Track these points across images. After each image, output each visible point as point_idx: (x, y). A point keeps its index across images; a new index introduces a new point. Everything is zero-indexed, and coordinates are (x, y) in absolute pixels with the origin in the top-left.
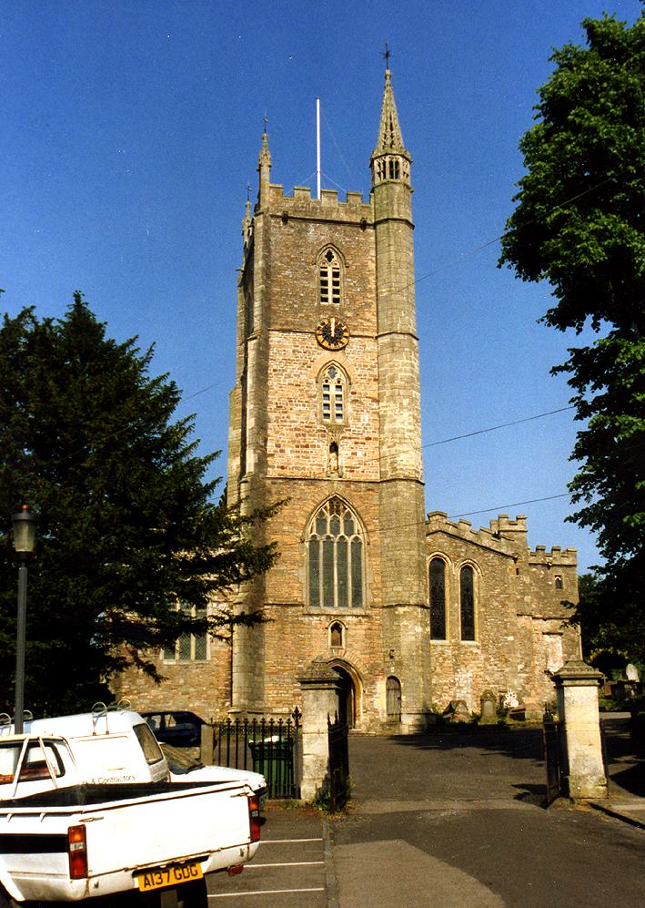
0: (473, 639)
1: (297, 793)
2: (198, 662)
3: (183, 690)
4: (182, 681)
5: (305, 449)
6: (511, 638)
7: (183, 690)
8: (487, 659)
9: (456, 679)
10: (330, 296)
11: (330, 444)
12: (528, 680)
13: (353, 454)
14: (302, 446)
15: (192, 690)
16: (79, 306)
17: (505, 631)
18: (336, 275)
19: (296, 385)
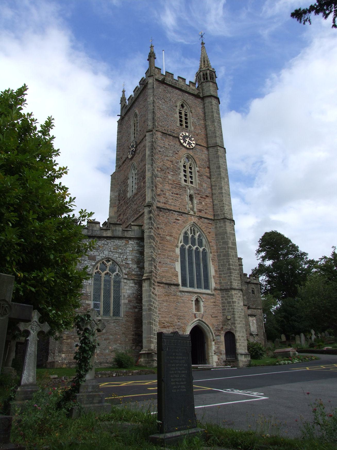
1: (235, 249)
2: (114, 318)
5: (176, 195)
13: (200, 203)
14: (175, 194)
15: (111, 337)
16: (22, 91)
19: (171, 161)
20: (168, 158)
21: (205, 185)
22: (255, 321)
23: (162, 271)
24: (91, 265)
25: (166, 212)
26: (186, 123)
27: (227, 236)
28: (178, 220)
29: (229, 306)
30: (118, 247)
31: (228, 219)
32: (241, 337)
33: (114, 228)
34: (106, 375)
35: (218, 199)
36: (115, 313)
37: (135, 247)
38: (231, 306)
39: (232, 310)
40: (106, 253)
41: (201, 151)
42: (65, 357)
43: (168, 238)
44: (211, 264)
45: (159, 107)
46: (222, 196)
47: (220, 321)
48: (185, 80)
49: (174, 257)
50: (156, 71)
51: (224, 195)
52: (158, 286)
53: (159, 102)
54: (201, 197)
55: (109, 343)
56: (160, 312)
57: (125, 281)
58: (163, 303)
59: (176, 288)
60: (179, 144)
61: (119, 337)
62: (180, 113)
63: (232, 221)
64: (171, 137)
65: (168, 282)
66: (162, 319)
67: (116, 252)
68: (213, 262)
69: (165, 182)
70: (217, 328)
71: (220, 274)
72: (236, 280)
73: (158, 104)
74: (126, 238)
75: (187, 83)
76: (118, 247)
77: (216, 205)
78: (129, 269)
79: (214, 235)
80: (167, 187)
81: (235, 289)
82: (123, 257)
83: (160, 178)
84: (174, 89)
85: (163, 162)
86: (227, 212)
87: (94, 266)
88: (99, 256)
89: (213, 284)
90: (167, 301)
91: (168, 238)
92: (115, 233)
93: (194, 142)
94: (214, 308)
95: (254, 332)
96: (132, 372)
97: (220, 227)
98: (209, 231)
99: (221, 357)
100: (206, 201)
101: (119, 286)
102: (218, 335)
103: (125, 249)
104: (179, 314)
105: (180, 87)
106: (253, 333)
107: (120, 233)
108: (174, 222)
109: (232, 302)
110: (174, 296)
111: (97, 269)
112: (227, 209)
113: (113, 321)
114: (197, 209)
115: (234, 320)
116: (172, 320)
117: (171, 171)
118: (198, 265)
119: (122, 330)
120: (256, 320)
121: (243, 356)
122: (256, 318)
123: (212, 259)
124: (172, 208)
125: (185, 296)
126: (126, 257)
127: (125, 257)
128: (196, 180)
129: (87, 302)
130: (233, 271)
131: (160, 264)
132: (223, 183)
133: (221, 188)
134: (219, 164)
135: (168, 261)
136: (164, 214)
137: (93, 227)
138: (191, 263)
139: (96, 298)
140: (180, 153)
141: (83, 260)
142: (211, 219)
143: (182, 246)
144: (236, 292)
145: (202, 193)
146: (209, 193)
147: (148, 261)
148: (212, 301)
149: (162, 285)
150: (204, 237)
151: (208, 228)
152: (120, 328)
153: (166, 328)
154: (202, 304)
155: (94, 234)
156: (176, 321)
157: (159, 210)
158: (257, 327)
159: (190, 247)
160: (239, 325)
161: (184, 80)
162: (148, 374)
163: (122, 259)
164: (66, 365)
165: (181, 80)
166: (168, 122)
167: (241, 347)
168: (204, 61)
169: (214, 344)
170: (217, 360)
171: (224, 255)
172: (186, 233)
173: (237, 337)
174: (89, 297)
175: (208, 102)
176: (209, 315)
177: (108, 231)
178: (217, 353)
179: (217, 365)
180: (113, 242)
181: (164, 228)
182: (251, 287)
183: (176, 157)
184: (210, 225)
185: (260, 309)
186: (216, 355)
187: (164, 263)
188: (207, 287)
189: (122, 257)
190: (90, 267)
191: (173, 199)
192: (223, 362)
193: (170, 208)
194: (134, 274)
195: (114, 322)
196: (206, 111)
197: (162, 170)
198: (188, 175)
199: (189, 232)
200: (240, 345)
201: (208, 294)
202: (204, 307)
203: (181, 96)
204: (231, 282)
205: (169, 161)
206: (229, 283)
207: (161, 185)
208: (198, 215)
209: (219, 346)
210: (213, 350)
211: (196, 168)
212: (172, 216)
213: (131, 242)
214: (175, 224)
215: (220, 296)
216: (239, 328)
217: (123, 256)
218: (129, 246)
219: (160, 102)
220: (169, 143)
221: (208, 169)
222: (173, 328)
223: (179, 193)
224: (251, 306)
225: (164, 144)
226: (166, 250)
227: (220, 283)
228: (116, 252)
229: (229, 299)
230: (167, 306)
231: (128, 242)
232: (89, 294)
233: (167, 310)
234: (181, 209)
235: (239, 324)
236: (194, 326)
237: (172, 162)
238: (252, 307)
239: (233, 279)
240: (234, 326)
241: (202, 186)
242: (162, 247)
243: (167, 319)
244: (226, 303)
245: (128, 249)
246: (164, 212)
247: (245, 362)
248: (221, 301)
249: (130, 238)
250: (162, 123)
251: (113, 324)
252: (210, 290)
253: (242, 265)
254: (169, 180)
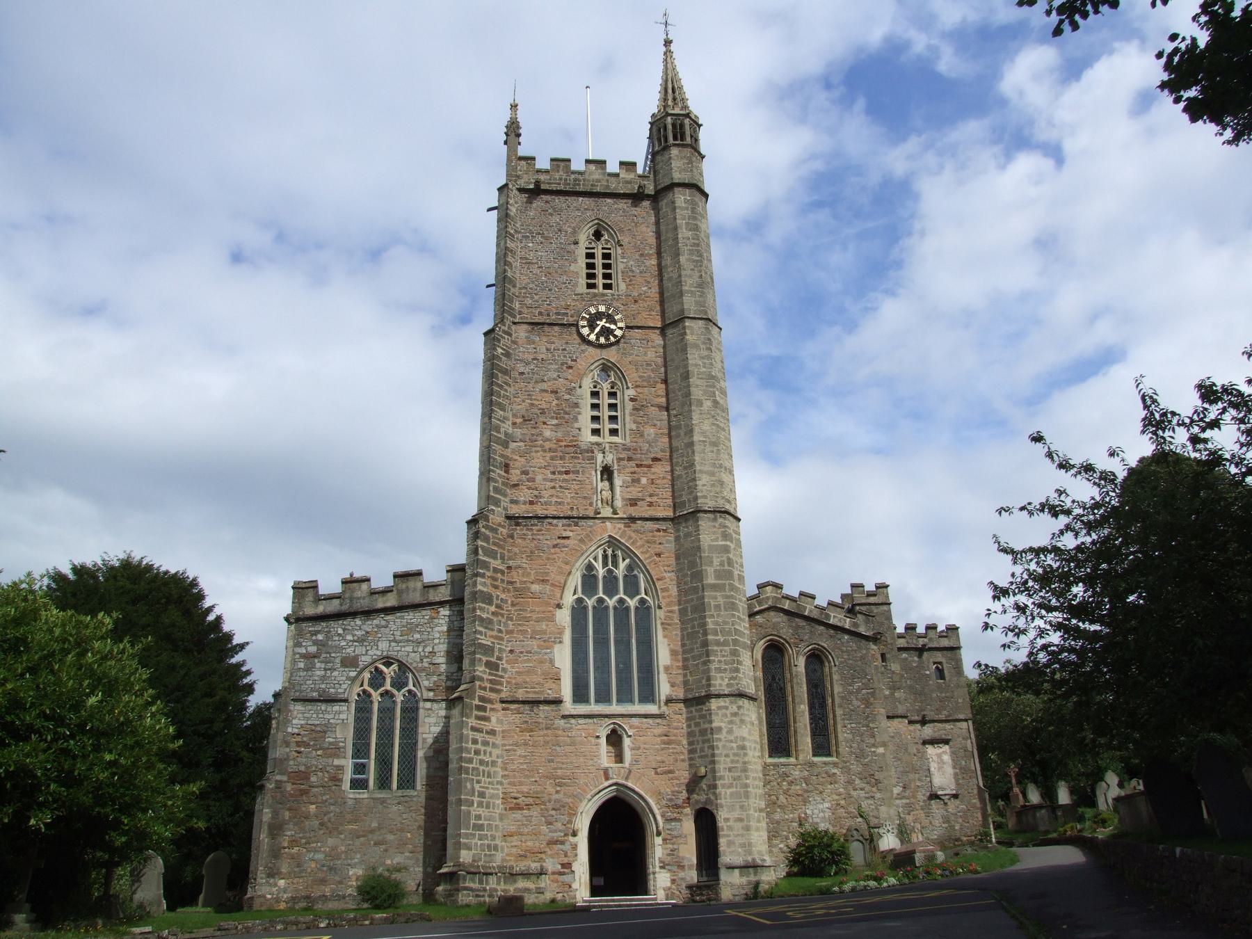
0: (829, 755)
2: (400, 793)
3: (376, 837)
4: (375, 825)
5: (565, 476)
6: (881, 750)
7: (376, 837)
8: (850, 782)
9: (809, 812)
11: (760, 646)
12: (909, 808)
13: (633, 481)
14: (560, 473)
15: (391, 837)
17: (872, 741)
18: (606, 256)
19: (552, 392)
20: (545, 386)
21: (650, 432)
22: (946, 758)
23: (516, 672)
25: (532, 525)
28: (568, 538)
29: (704, 742)
30: (411, 628)
31: (706, 512)
32: (735, 821)
33: (404, 586)
34: (297, 925)
36: (404, 782)
37: (455, 623)
38: (708, 741)
39: (710, 751)
40: (383, 645)
41: (645, 342)
42: (287, 885)
43: (536, 588)
45: (526, 259)
47: (681, 781)
48: (604, 162)
49: (550, 633)
50: (523, 166)
51: (697, 448)
53: (526, 247)
54: (638, 466)
55: (386, 850)
56: (506, 773)
57: (428, 705)
58: (515, 751)
59: (552, 711)
60: (578, 340)
61: (409, 835)
62: (590, 256)
63: (718, 515)
64: (556, 328)
65: (531, 696)
66: (513, 789)
67: (408, 641)
68: (664, 629)
69: (534, 449)
70: (671, 800)
71: (685, 660)
72: (726, 669)
73: (523, 253)
74: (430, 604)
75: (613, 167)
76: (411, 628)
77: (680, 477)
78: (439, 675)
79: (674, 559)
80: (539, 459)
81: (718, 696)
82: (423, 651)
83: (521, 441)
84: (573, 198)
85: (531, 400)
86: (705, 493)
87: (353, 680)
88: (366, 654)
89: (664, 688)
90: (526, 744)
91: (536, 588)
92: (404, 596)
93: (621, 324)
94: (662, 749)
95: (943, 789)
96: (372, 919)
97: (687, 535)
98: (657, 550)
99: (682, 874)
100: (654, 474)
101: (415, 719)
102: (675, 820)
103: (429, 630)
104: (559, 772)
105: (588, 189)
106: (939, 793)
107: (418, 594)
108: (555, 546)
111: (362, 685)
112: (705, 485)
113: (396, 802)
114: (623, 499)
115: (714, 778)
116: (539, 788)
117: (552, 418)
118: (623, 644)
119: (416, 821)
120: (953, 753)
121: (737, 871)
122: (951, 748)
123: (662, 624)
124: (552, 511)
125: (579, 727)
126: (431, 650)
127: (429, 649)
128: (628, 422)
129: (336, 762)
130: (715, 648)
131: (511, 656)
132: (694, 418)
133: (690, 432)
134: (686, 366)
136: (528, 529)
137: (353, 591)
138: (602, 642)
139: (358, 751)
140: (581, 364)
141: (329, 669)
142: (664, 519)
143: (579, 601)
144: (723, 704)
145: (642, 454)
146: (662, 451)
148: (657, 731)
150: (641, 569)
151: (655, 542)
153: (521, 809)
154: (627, 742)
155: (358, 606)
156: (552, 790)
157: (513, 523)
158: (956, 775)
160: (729, 791)
161: (602, 163)
162: (414, 921)
164: (287, 903)
165: (592, 167)
166: (550, 290)
167: (733, 848)
168: (671, 89)
169: (661, 842)
170: (669, 884)
171: (695, 609)
172: (590, 567)
173: (721, 823)
174: (342, 750)
176: (646, 768)
177: (389, 594)
178: (668, 865)
179: (667, 895)
180: (400, 618)
181: (524, 565)
182: (931, 660)
183: (569, 377)
184: (661, 533)
185: (966, 720)
186: (665, 871)
187: (521, 653)
188: (648, 695)
189: (420, 649)
190: (344, 683)
191: (554, 487)
192: (686, 887)
193: (546, 512)
195: (399, 803)
196: (663, 228)
197: (526, 420)
199: (599, 565)
200: (730, 843)
201: (646, 716)
202: (632, 749)
203: (593, 210)
204: (709, 679)
205: (546, 391)
206: (704, 682)
207: (522, 460)
208: (625, 516)
209: (675, 847)
210: (657, 859)
211: (625, 390)
212: (548, 530)
214: (557, 550)
215: (684, 716)
216: (728, 797)
217: (425, 647)
218: (441, 621)
219: (531, 245)
220: (549, 346)
221: (663, 386)
222: (542, 809)
223: (574, 467)
224: (931, 715)
225: (535, 352)
226: (527, 620)
227: (686, 683)
228: (408, 641)
229: (704, 723)
230: (525, 756)
231: (438, 613)
232: (341, 744)
233: (525, 766)
234: (577, 508)
235: (730, 786)
237: (557, 392)
238: (937, 717)
239: (716, 668)
241: (642, 436)
242: (518, 614)
243: (525, 789)
244: (697, 734)
245: (437, 629)
246: (525, 525)
247: (742, 886)
248: (685, 731)
249: (441, 604)
250: (532, 298)
251: (395, 808)
252: (656, 704)
253: (890, 604)
254: (547, 440)
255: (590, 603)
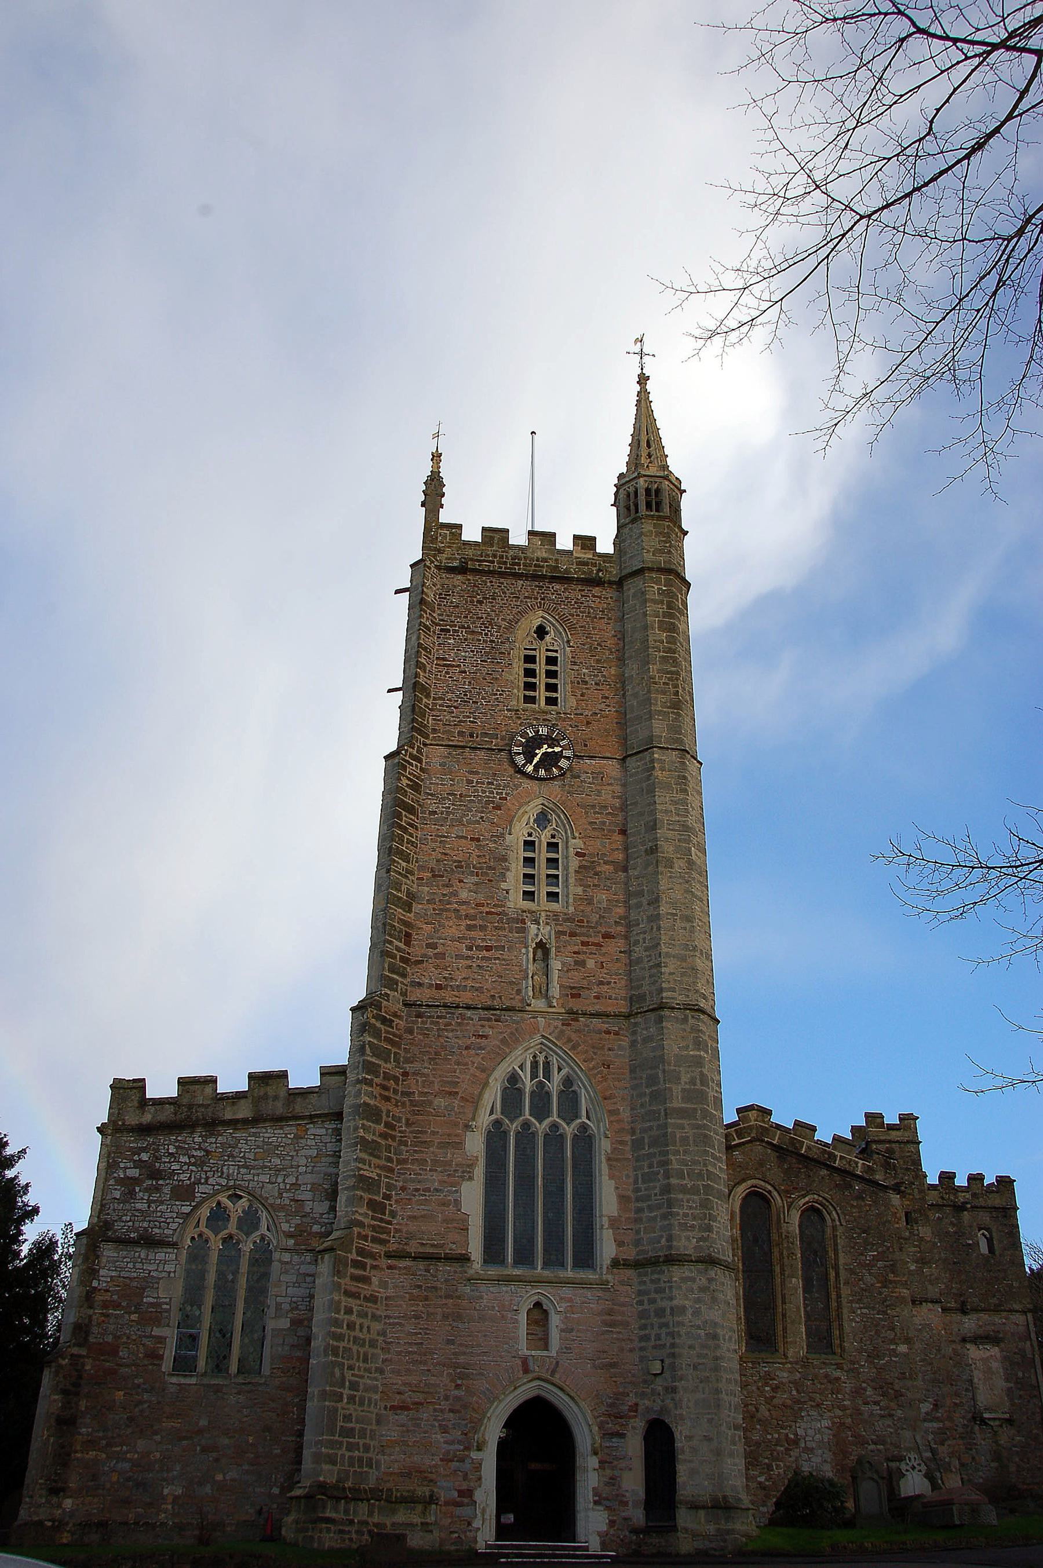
4: (203, 1423)
9: (800, 1432)
10: (542, 694)
13: (576, 963)
18: (552, 661)
19: (472, 839)
24: (179, 1215)
26: (551, 688)
27: (664, 1071)
28: (486, 1037)
35: (644, 939)
39: (669, 1341)
44: (605, 1178)
46: (659, 928)
52: (390, 1267)
55: (217, 1460)
60: (511, 771)
62: (530, 659)
68: (611, 1167)
72: (693, 1226)
77: (639, 961)
88: (206, 1183)
89: (607, 1248)
90: (417, 1317)
91: (440, 1102)
104: (462, 1359)
107: (279, 1104)
109: (668, 1311)
110: (448, 1297)
121: (702, 1513)
122: (1002, 1351)
127: (291, 1180)
129: (157, 1332)
130: (680, 1196)
133: (655, 901)
134: (653, 812)
135: (434, 1179)
136: (432, 1023)
143: (497, 1123)
147: (346, 1189)
149: (402, 1264)
151: (602, 1048)
152: (258, 1410)
159: (526, 1125)
163: (282, 1186)
172: (513, 1078)
175: (634, 595)
180: (254, 1135)
187: (417, 1190)
189: (280, 1180)
194: (317, 1233)
195: (239, 1393)
198: (542, 870)
213: (312, 1130)
222: (435, 1410)
229: (662, 1299)
232: (165, 1306)
234: (500, 997)
236: (521, 1401)
240: (673, 1399)
245: (303, 1152)
249: (312, 1118)
255: (541, 1128)
